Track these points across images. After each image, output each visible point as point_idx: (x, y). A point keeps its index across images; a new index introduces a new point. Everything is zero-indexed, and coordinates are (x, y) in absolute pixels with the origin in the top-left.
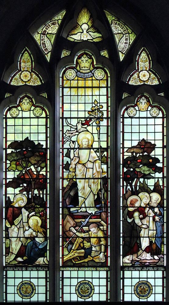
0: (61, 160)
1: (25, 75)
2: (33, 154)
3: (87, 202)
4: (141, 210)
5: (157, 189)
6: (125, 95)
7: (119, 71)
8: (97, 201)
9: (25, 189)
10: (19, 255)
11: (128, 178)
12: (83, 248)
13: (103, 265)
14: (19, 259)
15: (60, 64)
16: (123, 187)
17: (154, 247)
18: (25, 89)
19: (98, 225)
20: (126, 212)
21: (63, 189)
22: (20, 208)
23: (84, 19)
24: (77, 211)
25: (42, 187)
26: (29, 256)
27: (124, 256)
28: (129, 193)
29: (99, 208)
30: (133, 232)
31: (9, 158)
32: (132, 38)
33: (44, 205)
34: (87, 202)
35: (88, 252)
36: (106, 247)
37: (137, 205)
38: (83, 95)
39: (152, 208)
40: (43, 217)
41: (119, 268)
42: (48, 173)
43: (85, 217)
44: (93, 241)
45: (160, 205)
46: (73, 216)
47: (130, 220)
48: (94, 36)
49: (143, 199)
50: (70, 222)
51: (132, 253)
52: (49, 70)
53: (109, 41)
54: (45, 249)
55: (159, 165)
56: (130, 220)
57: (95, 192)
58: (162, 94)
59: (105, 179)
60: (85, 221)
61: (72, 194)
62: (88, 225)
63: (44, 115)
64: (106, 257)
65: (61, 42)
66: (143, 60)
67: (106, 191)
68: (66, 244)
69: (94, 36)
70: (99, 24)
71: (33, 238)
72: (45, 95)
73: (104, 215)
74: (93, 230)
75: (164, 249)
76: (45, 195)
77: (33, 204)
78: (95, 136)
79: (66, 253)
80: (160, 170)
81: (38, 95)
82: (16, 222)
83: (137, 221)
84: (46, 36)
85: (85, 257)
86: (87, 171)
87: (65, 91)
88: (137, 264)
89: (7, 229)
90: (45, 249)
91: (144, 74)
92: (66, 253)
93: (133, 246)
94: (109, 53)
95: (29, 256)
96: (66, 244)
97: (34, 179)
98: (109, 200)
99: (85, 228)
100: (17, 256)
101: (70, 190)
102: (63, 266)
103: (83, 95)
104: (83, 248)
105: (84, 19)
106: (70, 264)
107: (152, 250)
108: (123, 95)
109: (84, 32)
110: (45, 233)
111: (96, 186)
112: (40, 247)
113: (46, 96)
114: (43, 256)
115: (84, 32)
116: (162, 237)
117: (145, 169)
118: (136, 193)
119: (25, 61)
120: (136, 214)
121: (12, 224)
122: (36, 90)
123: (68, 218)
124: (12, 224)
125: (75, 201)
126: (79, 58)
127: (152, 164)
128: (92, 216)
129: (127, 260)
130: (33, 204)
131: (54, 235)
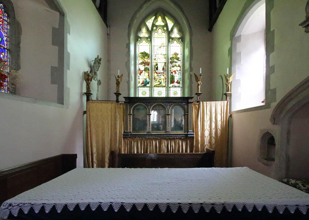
0: (153, 58)
1: (144, 33)
2: (146, 55)
3: (160, 70)
4: (175, 72)
5: (179, 66)
6: (171, 40)
7: (169, 33)
8: (163, 69)
9: (144, 65)
10: (142, 83)
11: (171, 63)
12: (159, 82)
13: (165, 86)
14: (142, 85)
15: (153, 31)
16: (170, 65)
17: (178, 82)
18: (144, 37)
19: (163, 75)
20: (171, 72)
21: (154, 65)
22: (142, 71)
23: (160, 19)
24: (186, 116)
25: (148, 65)
26: (145, 84)
27: (170, 84)
28: (172, 67)
29: (164, 71)
30: (173, 77)
31: (140, 57)
32: (173, 24)
33: (149, 70)
34: (160, 70)
35: (161, 83)
36: (165, 81)
37: (174, 70)
38: (160, 37)
39: (177, 71)
40: (149, 73)
41: (137, 87)
42: (166, 85)
43: (160, 73)
44: (162, 80)
45: (180, 70)
46: (156, 73)
47: (172, 74)
48: (163, 24)
49: (175, 69)
50: (156, 75)
51: (172, 83)
52: (150, 32)
53: (166, 25)
54: (149, 82)
55: (179, 59)
56: (172, 74)
57: (163, 66)
58: (180, 40)
59: (165, 63)
60: (160, 74)
61: (156, 67)
62: (160, 75)
63: (149, 45)
64: (165, 84)
65: (153, 25)
66: (176, 30)
67: (165, 66)
68: (155, 81)
69: (163, 24)
70: (164, 20)
71: (146, 79)
72: (149, 39)
73: (165, 73)
74: (162, 76)
75: (181, 82)
76: (149, 67)
77: (146, 70)
78: (163, 51)
79: (155, 83)
80: (180, 60)
81: (147, 39)
82: (141, 74)
83: (174, 75)
84: (149, 23)
85: (160, 84)
86: (161, 62)
87: (189, 169)
88: (174, 86)
89: (139, 76)
90: (149, 82)
91: (176, 34)
92: (155, 83)
93: (172, 82)
94: (166, 29)
95: (145, 84)
96: (155, 81)
97: (146, 63)
98: (166, 69)
99: (160, 76)
100: (141, 84)
101: (156, 65)
102: (154, 87)
103: (160, 37)
104: (159, 82)
105: (160, 19)
106: (156, 86)
107: (178, 83)
108: (170, 39)
109: (160, 22)
110: (149, 78)
111: (163, 64)
112: (148, 81)
113: (150, 39)
114: (148, 84)
115: (160, 22)
116: (180, 79)
117: (176, 60)
118: (173, 67)
119: (144, 30)
120: (174, 73)
121: (140, 75)
122: (147, 38)
123: (155, 73)
124: (140, 75)
125: (157, 69)
126: (158, 29)
127: (178, 59)
128: (162, 73)
129: (171, 85)
130: (146, 70)
131: (151, 78)
